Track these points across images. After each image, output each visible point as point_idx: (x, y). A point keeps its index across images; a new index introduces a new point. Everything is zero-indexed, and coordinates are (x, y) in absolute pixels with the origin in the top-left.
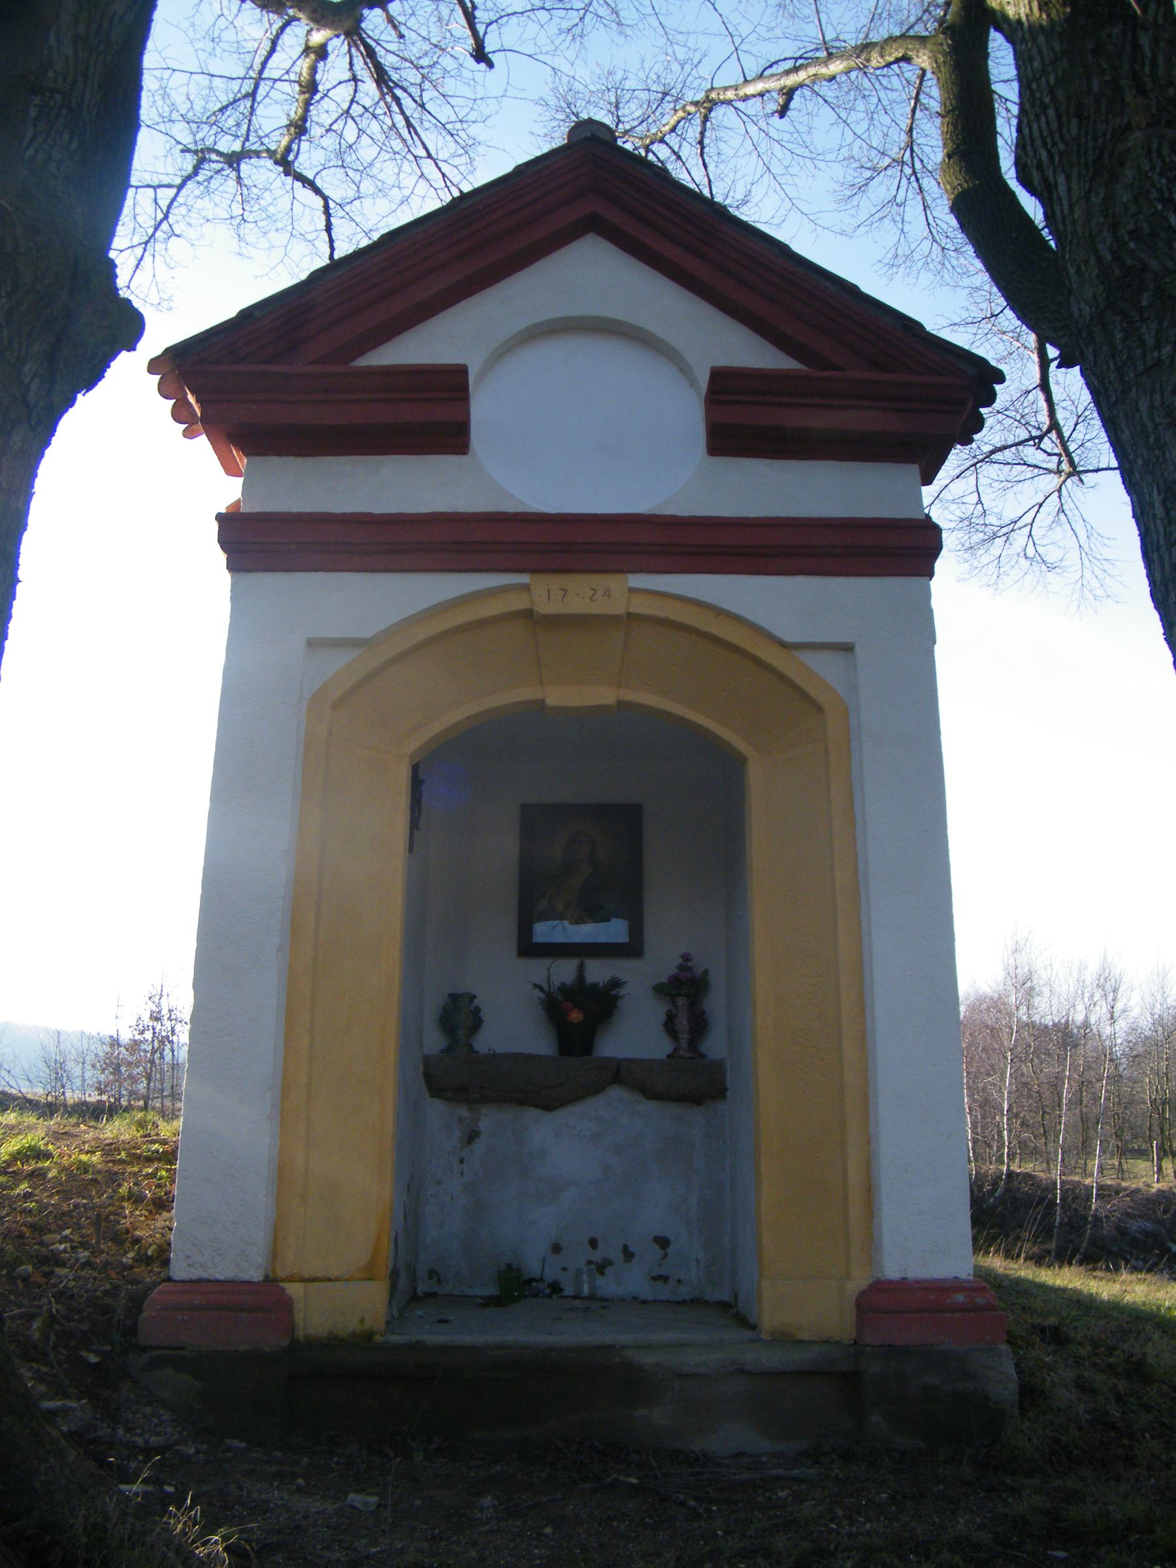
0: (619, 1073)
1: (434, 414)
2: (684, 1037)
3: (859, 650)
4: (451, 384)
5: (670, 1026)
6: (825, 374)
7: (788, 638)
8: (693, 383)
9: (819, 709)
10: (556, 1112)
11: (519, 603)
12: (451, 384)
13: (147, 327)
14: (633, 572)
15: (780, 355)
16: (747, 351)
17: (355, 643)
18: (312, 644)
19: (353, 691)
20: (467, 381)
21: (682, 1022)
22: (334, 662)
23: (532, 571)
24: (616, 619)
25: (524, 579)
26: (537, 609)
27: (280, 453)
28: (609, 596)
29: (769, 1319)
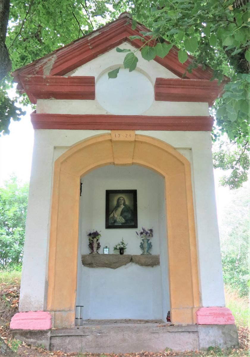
0: (131, 259)
1: (85, 89)
2: (146, 250)
3: (193, 149)
4: (90, 82)
5: (142, 246)
6: (185, 80)
7: (175, 147)
8: (152, 82)
9: (183, 164)
10: (116, 269)
11: (109, 138)
12: (90, 82)
13: (116, 78)
14: (137, 130)
15: (174, 75)
16: (167, 75)
17: (66, 147)
18: (55, 148)
19: (65, 161)
20: (95, 81)
21: (146, 245)
22: (59, 154)
23: (111, 130)
24: (130, 142)
25: (109, 132)
26: (112, 139)
27: (202, 117)
28: (131, 136)
29: (220, 331)
